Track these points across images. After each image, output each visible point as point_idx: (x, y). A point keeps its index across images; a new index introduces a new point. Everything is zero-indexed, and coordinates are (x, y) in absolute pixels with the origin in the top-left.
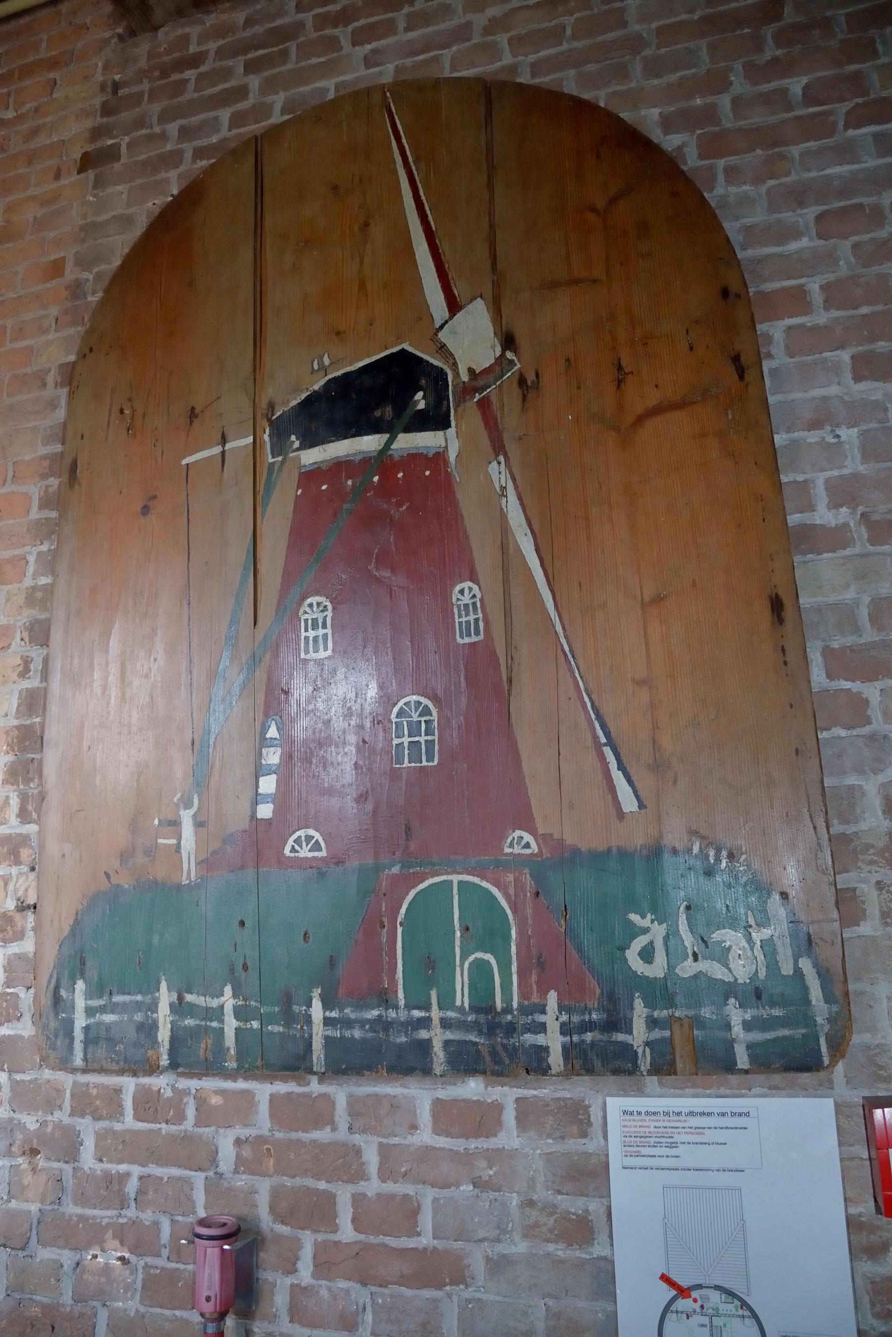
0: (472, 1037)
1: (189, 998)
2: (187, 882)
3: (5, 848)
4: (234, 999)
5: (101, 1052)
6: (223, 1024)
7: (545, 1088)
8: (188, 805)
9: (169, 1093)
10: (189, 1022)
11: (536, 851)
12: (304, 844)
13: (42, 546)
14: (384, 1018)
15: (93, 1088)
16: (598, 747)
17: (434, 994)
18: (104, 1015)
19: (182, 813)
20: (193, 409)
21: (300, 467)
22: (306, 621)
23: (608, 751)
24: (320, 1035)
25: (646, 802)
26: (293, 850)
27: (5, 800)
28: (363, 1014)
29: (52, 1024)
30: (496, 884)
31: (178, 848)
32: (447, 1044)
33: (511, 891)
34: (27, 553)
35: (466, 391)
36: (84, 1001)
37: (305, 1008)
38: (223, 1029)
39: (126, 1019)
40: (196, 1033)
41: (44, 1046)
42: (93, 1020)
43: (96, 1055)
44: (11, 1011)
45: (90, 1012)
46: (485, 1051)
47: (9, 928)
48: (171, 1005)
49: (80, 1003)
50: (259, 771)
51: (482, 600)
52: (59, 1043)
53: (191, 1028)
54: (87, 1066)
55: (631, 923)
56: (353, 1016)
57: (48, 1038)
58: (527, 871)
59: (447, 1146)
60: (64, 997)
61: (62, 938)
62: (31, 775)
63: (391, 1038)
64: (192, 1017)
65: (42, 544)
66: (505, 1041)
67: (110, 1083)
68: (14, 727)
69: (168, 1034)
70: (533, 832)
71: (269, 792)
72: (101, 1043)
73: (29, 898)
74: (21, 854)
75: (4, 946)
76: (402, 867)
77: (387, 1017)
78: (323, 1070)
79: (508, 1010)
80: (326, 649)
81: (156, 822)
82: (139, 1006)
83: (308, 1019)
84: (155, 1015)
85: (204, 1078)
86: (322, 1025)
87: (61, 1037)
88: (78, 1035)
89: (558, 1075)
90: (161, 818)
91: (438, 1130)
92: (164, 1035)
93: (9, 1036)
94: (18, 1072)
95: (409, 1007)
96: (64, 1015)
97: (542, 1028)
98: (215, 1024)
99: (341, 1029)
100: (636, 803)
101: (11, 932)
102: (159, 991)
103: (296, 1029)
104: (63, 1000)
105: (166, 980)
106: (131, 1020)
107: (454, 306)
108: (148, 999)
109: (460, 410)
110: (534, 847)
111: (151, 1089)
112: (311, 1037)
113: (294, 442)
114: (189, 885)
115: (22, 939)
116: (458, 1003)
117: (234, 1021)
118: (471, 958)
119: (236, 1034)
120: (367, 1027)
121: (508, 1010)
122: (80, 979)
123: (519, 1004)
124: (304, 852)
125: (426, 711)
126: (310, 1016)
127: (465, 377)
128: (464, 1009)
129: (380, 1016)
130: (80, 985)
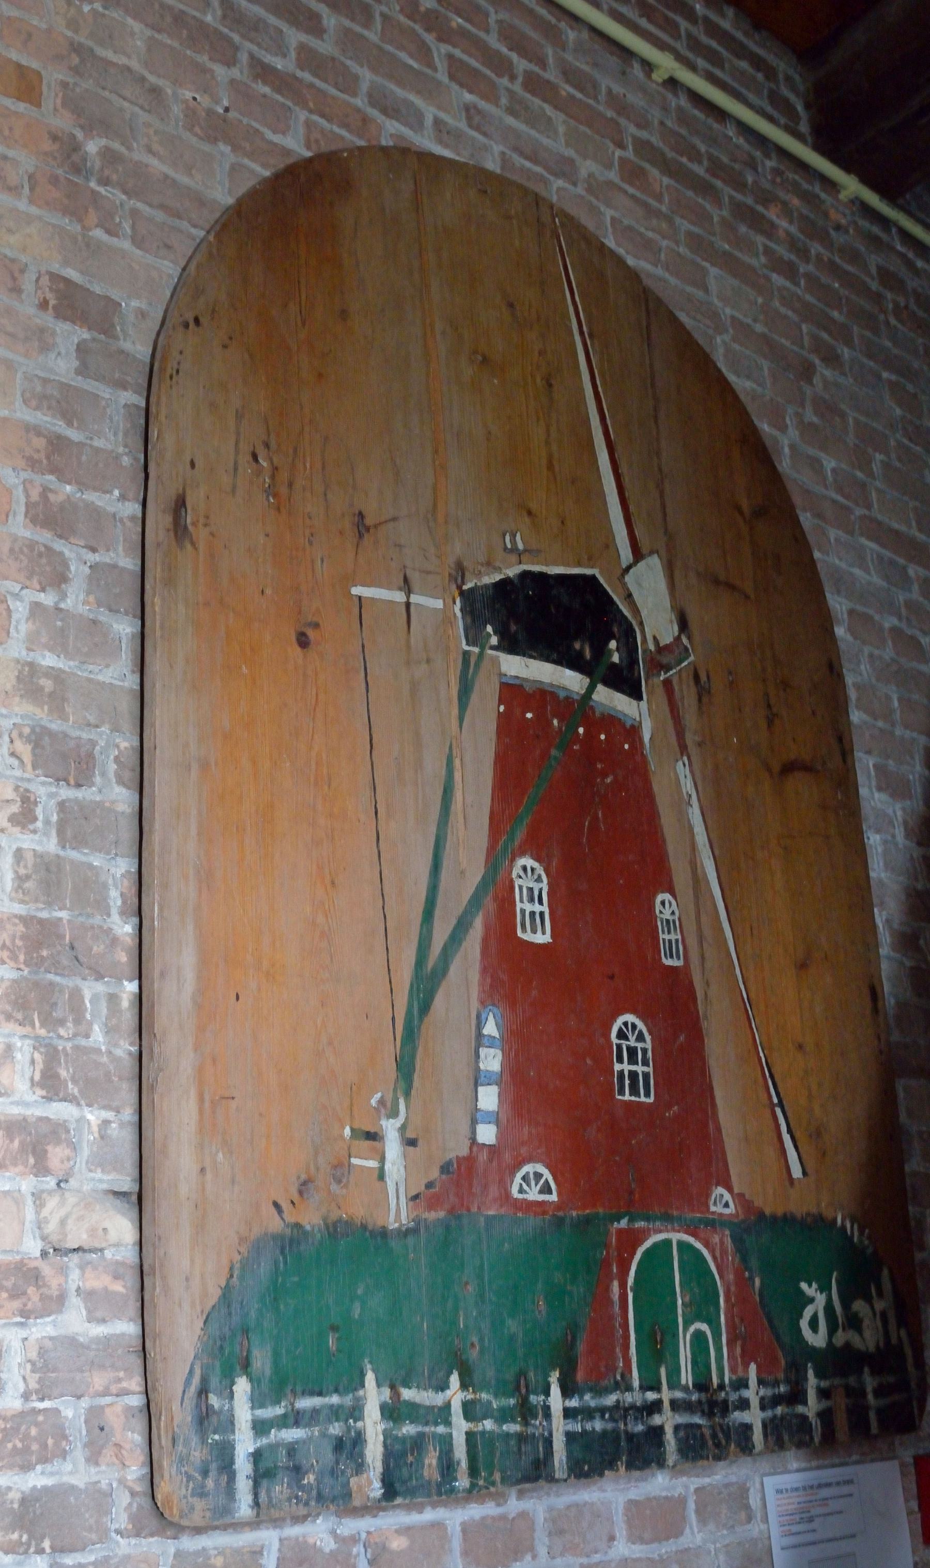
0: (697, 1420)
1: (407, 1394)
2: (397, 1225)
3: (16, 1143)
4: (463, 1391)
5: (280, 1489)
6: (451, 1428)
7: (716, 1474)
8: (394, 1114)
9: (329, 1545)
10: (409, 1429)
11: (734, 1211)
12: (533, 1183)
13: (42, 595)
14: (621, 1404)
15: (216, 1556)
16: (772, 1106)
17: (663, 1371)
18: (284, 1430)
19: (384, 1122)
20: (361, 515)
21: (501, 675)
22: (521, 887)
23: (778, 1111)
24: (561, 1430)
25: (808, 1170)
26: (521, 1191)
27: (5, 1051)
28: (602, 1400)
29: (197, 1454)
30: (707, 1245)
31: (381, 1175)
32: (677, 1428)
33: (718, 1254)
34: (12, 594)
35: (656, 666)
36: (250, 1411)
37: (543, 1397)
38: (451, 1435)
39: (317, 1433)
40: (418, 1444)
41: (184, 1491)
42: (265, 1441)
43: (273, 1495)
44: (50, 1442)
45: (260, 1427)
46: (707, 1432)
47: (31, 1290)
48: (383, 1408)
49: (243, 1414)
50: (477, 1079)
51: (679, 919)
52: (210, 1483)
53: (411, 1437)
54: (258, 1515)
55: (801, 1293)
56: (593, 1404)
57: (189, 1478)
58: (727, 1232)
59: (643, 1555)
60: (216, 1406)
61: (208, 1308)
62: (57, 1014)
63: (629, 1427)
64: (411, 1423)
65: (43, 590)
66: (721, 1421)
67: (241, 1543)
68: (16, 916)
69: (380, 1449)
70: (730, 1189)
71: (491, 1109)
72: (279, 1476)
73: (69, 1237)
74: (49, 1155)
75: (22, 1325)
76: (629, 1221)
77: (624, 1402)
78: (565, 1476)
79: (721, 1387)
80: (544, 933)
81: (347, 1131)
82: (335, 1413)
83: (547, 1410)
84: (360, 1424)
85: (381, 1513)
86: (562, 1418)
87: (213, 1474)
88: (243, 1466)
89: (760, 1454)
90: (356, 1126)
91: (635, 1538)
92: (374, 1451)
93: (45, 1489)
94: (72, 1550)
95: (644, 1388)
96: (217, 1437)
97: (744, 1404)
98: (441, 1429)
99: (582, 1421)
100: (800, 1171)
101: (36, 1298)
102: (364, 1386)
103: (534, 1426)
104: (214, 1412)
105: (373, 1370)
106: (324, 1435)
107: (638, 555)
108: (348, 1400)
109: (650, 682)
110: (731, 1209)
111: (306, 1542)
112: (551, 1435)
113: (489, 635)
114: (399, 1230)
115: (59, 1311)
116: (683, 1382)
117: (463, 1422)
118: (692, 1329)
119: (467, 1440)
120: (607, 1416)
121: (721, 1387)
122: (240, 1376)
123: (730, 1379)
124: (533, 1194)
125: (641, 1038)
126: (548, 1407)
127: (652, 647)
128: (689, 1388)
129: (618, 1401)
130: (242, 1386)
